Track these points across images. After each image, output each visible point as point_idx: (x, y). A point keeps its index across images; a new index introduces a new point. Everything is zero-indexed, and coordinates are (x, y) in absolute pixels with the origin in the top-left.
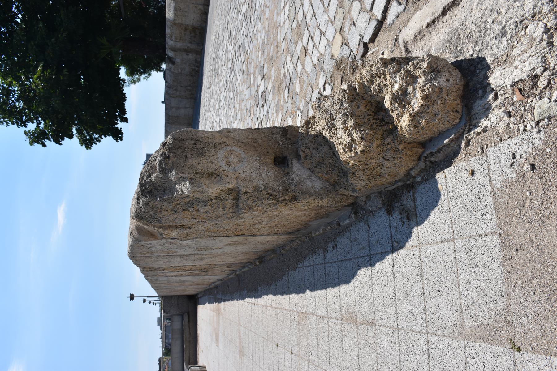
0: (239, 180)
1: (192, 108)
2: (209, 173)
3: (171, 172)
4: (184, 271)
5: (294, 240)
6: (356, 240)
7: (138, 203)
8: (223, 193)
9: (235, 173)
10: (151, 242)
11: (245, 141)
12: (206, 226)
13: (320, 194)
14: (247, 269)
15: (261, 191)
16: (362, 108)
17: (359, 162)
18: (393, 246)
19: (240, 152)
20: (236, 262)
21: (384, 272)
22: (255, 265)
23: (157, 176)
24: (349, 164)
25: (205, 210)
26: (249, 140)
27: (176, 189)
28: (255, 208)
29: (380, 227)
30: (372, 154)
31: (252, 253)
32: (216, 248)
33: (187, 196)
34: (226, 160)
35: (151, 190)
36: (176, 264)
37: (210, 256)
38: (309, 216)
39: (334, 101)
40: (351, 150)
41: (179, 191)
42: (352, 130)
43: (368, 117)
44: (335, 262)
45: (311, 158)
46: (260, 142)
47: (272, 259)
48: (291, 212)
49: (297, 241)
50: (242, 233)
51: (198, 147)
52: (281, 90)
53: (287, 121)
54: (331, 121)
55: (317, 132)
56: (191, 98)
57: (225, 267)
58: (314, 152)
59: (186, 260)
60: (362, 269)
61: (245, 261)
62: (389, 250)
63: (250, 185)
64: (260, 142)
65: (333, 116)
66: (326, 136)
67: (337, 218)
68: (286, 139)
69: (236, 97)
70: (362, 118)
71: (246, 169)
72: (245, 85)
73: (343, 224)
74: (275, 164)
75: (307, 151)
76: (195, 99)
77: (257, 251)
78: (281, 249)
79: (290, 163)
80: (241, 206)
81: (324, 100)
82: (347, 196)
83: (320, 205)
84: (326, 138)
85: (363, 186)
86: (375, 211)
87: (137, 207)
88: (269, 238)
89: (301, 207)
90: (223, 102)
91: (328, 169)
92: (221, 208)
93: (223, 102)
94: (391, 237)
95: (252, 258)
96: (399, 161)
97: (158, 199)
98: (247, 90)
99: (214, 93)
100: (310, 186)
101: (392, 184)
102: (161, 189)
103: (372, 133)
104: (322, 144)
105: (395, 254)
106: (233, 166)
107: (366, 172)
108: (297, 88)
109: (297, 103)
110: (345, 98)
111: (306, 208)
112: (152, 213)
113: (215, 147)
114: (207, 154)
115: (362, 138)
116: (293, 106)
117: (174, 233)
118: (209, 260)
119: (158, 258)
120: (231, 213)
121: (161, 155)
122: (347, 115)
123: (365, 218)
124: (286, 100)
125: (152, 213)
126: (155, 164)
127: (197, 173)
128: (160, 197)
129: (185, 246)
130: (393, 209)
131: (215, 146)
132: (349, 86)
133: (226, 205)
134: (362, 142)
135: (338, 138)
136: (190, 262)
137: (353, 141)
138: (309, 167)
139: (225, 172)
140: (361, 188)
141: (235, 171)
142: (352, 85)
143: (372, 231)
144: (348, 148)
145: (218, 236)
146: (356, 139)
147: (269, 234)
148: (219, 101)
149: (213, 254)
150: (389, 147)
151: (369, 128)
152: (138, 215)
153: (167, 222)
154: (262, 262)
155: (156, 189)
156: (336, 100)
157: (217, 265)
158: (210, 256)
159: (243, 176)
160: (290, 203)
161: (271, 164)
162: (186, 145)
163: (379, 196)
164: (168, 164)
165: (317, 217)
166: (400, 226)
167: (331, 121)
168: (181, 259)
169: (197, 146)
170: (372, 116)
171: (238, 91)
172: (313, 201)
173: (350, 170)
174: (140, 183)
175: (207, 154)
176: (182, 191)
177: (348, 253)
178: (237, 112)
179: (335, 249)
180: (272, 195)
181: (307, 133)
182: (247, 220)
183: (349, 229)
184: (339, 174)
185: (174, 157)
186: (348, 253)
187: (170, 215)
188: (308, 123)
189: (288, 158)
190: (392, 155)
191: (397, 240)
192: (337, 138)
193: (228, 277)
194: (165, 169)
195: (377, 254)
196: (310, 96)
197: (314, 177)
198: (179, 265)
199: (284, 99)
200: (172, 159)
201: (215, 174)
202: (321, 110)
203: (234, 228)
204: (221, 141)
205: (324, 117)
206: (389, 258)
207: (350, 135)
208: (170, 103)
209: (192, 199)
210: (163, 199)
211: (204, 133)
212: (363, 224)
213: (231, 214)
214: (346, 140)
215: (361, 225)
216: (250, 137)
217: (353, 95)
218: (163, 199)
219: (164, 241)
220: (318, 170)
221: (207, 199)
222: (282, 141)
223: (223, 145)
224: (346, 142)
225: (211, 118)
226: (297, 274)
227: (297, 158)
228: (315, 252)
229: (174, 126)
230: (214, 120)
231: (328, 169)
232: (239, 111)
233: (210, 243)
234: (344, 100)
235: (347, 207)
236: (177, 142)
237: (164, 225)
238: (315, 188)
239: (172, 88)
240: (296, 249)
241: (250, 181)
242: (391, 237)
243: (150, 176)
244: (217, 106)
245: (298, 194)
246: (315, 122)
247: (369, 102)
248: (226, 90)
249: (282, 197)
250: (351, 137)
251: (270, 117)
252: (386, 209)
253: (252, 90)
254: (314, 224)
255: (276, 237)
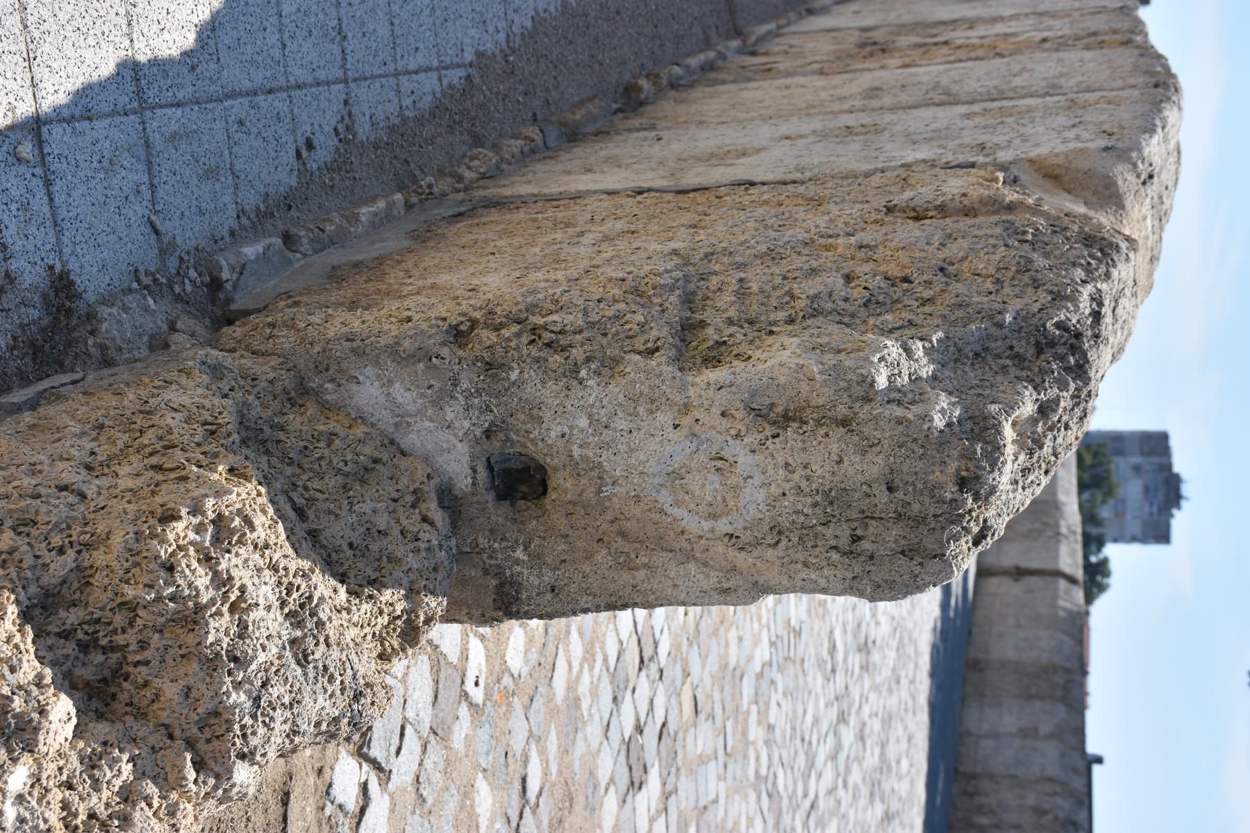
0: (679, 398)
1: (969, 734)
2: (795, 425)
3: (949, 425)
4: (959, 42)
5: (483, 176)
6: (211, 173)
7: (1097, 299)
8: (745, 348)
9: (697, 429)
10: (1061, 148)
11: (660, 558)
12: (822, 221)
13: (358, 353)
14: (694, 62)
15: (588, 360)
16: (171, 691)
17: (185, 479)
18: (40, 143)
19: (677, 512)
20: (733, 87)
21: (74, 36)
22: (657, 76)
23: (1010, 407)
24: (231, 470)
25: (818, 279)
26: (644, 560)
27: (932, 361)
28: (616, 291)
29: (103, 227)
30: (131, 507)
31: (663, 124)
32: (801, 136)
33: (891, 331)
34: (732, 480)
35: (1040, 351)
36: (980, 68)
37: (836, 107)
38: (407, 271)
39: (288, 714)
40: (219, 521)
41: (920, 353)
42: (212, 601)
43: (147, 654)
44: (299, 87)
45: (395, 495)
46: (601, 556)
47: (582, 103)
48: (476, 281)
49: (468, 175)
50: (685, 201)
51: (845, 526)
52: (559, 792)
53: (527, 662)
54: (305, 636)
55: (371, 597)
56: (973, 777)
57: (784, 64)
58: (382, 522)
59: (937, 85)
60: (175, 52)
61: (698, 92)
62: (57, 130)
63: (633, 381)
64: (601, 556)
65: (295, 656)
66: (333, 582)
67: (297, 266)
68: (499, 573)
69: (763, 772)
70: (171, 652)
71: (653, 445)
72: (725, 819)
73: (268, 241)
74: (542, 469)
75: (411, 523)
76: (956, 771)
77: (641, 134)
78: (540, 143)
79: (483, 474)
80: (673, 299)
81: (336, 720)
82: (247, 348)
83: (359, 313)
84: (333, 575)
85: (174, 387)
86: (130, 290)
87: (1104, 286)
88: (582, 183)
89: (433, 300)
90: (822, 754)
91: (327, 452)
92: (755, 288)
93: (822, 754)
94: (48, 184)
95: (666, 107)
96: (15, 483)
97: (1008, 318)
98: (712, 797)
99: (864, 791)
100: (397, 385)
101: (53, 396)
102: (998, 356)
103: (130, 592)
104: (349, 553)
105: (25, 109)
106: (703, 457)
107: (161, 438)
108: (485, 799)
109: (484, 734)
110: (243, 727)
111: (414, 298)
112: (1040, 261)
113: (778, 531)
114: (809, 500)
115: (170, 568)
116: (501, 723)
117: (954, 185)
118: (844, 91)
119: (1053, 86)
120: (715, 273)
121: (993, 490)
122: (235, 659)
123: (173, 263)
124: (533, 746)
125: (1040, 261)
126: (1022, 457)
127: (845, 423)
128: (1000, 325)
129: (927, 140)
130: (45, 296)
131: (780, 533)
132: (224, 775)
133: (733, 303)
134: (173, 554)
135: (274, 568)
136: (925, 79)
137: (208, 559)
138: (403, 463)
139: (733, 432)
140: (183, 380)
141: (694, 435)
142: (212, 781)
143: (138, 209)
144: (232, 532)
145: (785, 183)
146: (195, 564)
147: (577, 197)
148: (842, 757)
149: (818, 114)
150: (57, 540)
151: (141, 612)
152: (1105, 254)
153: (980, 227)
154: (626, 89)
155: (1019, 359)
156: (279, 720)
157: (814, 73)
158: (836, 107)
159: (665, 418)
160: (477, 315)
161: (556, 469)
162: (893, 534)
163: (112, 353)
164: (962, 456)
165: (378, 266)
166: (12, 226)
167: (305, 636)
168: (955, 89)
169: (848, 533)
170: (132, 658)
171: (752, 796)
172: (386, 327)
173: (230, 449)
174: (1087, 381)
175: (809, 500)
176: (908, 351)
177: (241, 123)
178: (754, 708)
179: (301, 142)
180: (549, 345)
181: (412, 594)
182: (654, 246)
183: (244, 220)
184: (282, 436)
185: (940, 486)
186: (241, 123)
187: (964, 258)
188: (411, 634)
189: (490, 497)
190: (44, 508)
191: (22, 169)
192: (277, 571)
193: (779, 27)
194: (974, 437)
195: (110, 115)
196: (428, 764)
197: (386, 420)
198: (970, 64)
199: (543, 752)
200: (944, 477)
201: (774, 423)
202: (348, 679)
203: (713, 217)
204: (756, 553)
205: (335, 653)
206: (55, 93)
207: (222, 582)
208: (1063, 755)
209: (871, 321)
210: (991, 317)
211: (822, 582)
212: (179, 240)
213: (717, 268)
214: (239, 561)
215: (188, 234)
216: (641, 574)
217: (208, 741)
218: (991, 317)
219: (1004, 156)
220: (367, 450)
221: (809, 322)
222: (518, 562)
223: (746, 537)
224: (237, 555)
225: (875, 688)
226: (468, 40)
227: (456, 497)
228: (392, 129)
229: (1045, 658)
230: (861, 678)
231: (327, 452)
232: (748, 712)
233: (818, 157)
234: (248, 721)
235: (251, 307)
236: (929, 543)
237: (996, 218)
238: (378, 376)
239: (1056, 818)
240: (478, 141)
241: (634, 399)
242: (48, 184)
243: (1045, 410)
244: (848, 736)
245: (445, 352)
246: (382, 640)
247: (141, 715)
248: (808, 803)
249: (509, 340)
250: (216, 574)
251: (606, 679)
252: (80, 297)
253: (692, 799)
254: (392, 241)
255: (554, 189)
